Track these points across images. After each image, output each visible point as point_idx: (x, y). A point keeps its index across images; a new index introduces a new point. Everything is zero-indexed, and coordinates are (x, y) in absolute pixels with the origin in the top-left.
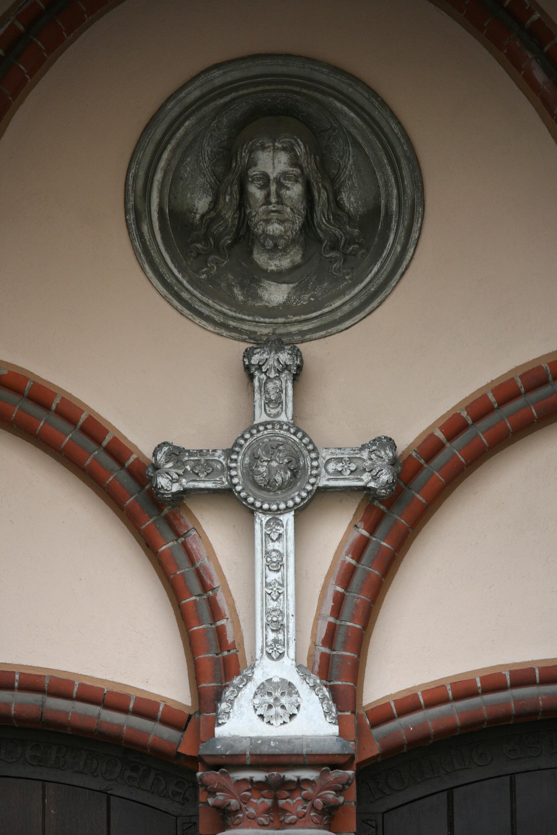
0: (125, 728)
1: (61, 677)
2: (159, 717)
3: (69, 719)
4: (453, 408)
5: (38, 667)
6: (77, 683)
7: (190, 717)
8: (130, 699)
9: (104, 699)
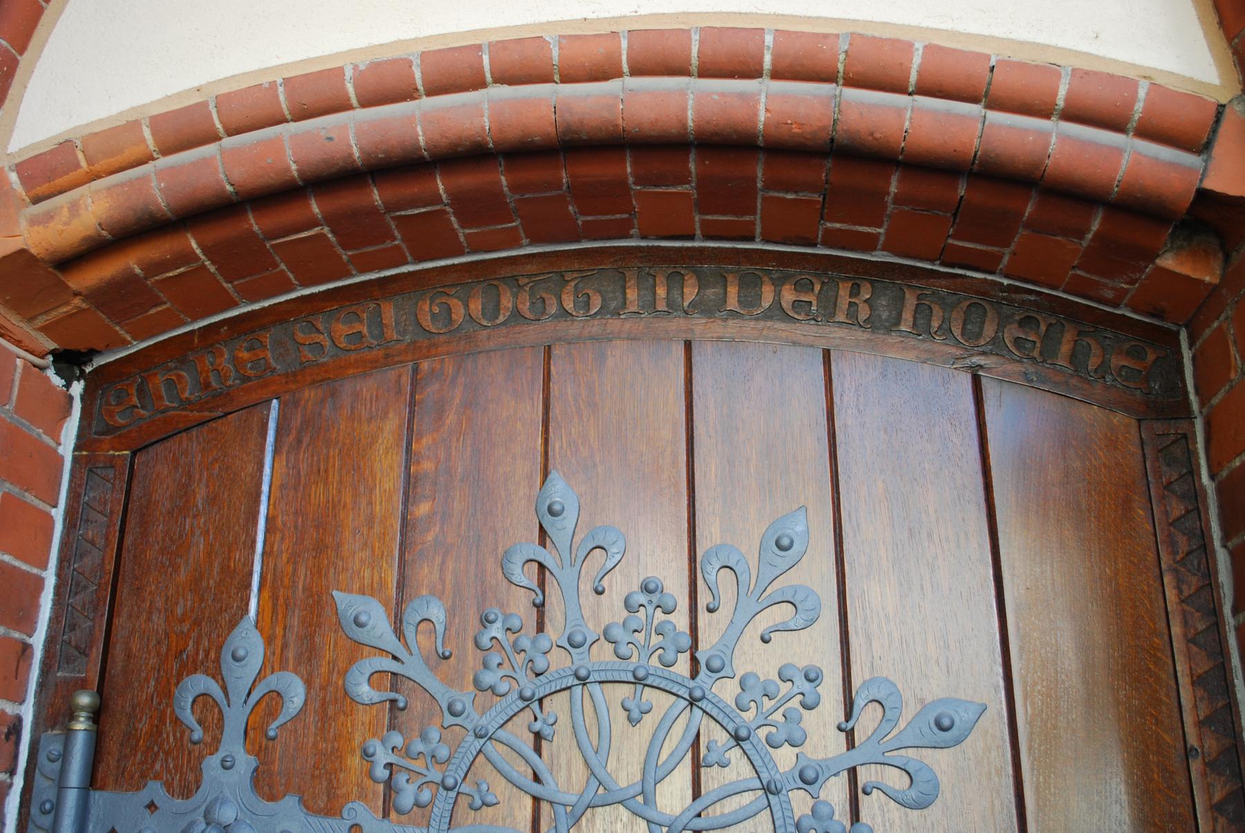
0: (1054, 140)
1: (877, 34)
2: (1136, 117)
3: (907, 124)
4: (541, 25)
5: (818, 18)
6: (919, 46)
7: (1220, 109)
8: (1059, 76)
9: (990, 84)
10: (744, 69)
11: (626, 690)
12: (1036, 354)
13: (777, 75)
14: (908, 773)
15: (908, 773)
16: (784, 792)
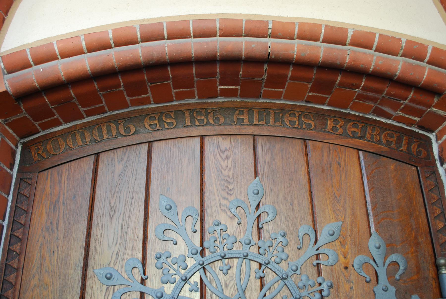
10: (184, 35)
11: (219, 263)
12: (158, 127)
13: (195, 37)
14: (133, 268)
15: (133, 268)
16: (249, 253)
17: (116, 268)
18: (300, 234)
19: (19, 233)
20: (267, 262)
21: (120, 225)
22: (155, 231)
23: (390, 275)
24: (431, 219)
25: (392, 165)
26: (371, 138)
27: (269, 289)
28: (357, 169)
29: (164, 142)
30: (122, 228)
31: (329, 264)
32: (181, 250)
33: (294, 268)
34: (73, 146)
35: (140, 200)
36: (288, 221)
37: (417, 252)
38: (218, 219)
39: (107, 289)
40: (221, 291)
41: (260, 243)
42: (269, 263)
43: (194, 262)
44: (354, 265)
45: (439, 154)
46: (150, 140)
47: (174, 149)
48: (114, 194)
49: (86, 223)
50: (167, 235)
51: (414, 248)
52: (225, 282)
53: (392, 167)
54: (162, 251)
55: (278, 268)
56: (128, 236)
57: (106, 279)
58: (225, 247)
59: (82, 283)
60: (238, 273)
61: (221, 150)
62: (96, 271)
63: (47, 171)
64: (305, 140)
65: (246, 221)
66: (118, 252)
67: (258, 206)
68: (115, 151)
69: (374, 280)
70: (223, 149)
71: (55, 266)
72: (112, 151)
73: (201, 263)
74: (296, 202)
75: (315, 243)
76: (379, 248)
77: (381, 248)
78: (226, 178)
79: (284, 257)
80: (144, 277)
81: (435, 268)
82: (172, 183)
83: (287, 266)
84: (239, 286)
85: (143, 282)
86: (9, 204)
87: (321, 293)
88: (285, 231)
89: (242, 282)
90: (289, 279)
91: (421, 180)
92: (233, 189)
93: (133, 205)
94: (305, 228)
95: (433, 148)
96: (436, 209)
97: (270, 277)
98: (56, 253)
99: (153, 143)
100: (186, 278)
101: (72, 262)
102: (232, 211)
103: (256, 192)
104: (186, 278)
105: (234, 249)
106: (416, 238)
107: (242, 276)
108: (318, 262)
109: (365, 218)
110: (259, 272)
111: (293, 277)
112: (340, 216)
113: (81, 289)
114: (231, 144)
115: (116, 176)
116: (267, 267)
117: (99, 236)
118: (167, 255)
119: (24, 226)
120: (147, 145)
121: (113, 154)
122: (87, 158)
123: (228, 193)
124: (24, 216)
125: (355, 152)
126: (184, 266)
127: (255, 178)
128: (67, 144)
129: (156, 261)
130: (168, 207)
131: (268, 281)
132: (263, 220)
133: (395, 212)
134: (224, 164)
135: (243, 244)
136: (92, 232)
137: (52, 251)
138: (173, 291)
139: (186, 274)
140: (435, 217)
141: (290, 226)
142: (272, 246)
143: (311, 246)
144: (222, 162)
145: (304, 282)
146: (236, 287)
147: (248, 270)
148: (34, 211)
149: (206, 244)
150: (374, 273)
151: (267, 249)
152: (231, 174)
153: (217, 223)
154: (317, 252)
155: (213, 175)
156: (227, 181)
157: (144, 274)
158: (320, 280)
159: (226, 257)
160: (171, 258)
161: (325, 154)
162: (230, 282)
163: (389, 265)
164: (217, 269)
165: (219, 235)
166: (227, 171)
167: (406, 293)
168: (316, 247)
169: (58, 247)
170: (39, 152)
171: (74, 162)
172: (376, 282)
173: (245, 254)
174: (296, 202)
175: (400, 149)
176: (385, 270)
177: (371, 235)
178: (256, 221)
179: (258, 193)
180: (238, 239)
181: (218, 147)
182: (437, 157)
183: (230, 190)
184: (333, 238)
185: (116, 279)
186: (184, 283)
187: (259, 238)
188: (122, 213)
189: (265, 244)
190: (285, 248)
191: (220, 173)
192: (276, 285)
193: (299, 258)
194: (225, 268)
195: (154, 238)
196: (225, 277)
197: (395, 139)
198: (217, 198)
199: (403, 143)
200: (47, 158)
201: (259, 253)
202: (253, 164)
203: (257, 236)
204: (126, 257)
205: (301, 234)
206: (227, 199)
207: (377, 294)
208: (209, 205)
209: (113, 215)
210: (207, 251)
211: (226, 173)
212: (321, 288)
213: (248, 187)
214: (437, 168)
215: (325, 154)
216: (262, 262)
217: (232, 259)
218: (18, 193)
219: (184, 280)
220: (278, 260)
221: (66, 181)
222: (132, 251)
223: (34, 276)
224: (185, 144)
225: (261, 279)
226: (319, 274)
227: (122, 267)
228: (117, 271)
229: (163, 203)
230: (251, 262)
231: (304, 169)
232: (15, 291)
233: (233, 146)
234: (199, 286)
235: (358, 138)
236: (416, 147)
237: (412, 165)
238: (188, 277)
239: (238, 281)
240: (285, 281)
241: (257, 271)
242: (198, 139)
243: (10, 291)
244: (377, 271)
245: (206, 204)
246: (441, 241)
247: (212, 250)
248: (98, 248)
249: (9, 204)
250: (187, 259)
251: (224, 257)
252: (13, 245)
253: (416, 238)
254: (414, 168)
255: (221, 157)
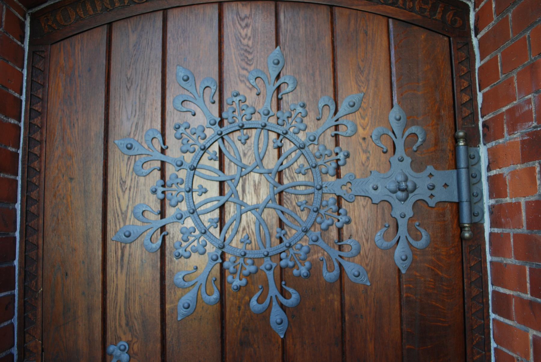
11: (237, 134)
16: (267, 123)
17: (136, 138)
18: (320, 105)
19: (38, 107)
20: (284, 132)
21: (138, 97)
22: (173, 102)
23: (407, 146)
24: (457, 92)
25: (423, 35)
26: (403, 5)
27: (286, 158)
28: (385, 38)
29: (179, 9)
30: (140, 100)
31: (348, 135)
32: (200, 120)
33: (312, 138)
34: (84, 15)
35: (157, 71)
36: (308, 92)
37: (438, 124)
38: (236, 90)
39: (129, 158)
40: (239, 160)
41: (279, 114)
42: (287, 133)
43: (213, 132)
44: (373, 137)
45: (475, 23)
46: (164, 7)
47: (191, 17)
48: (130, 66)
49: (104, 95)
50: (186, 106)
51: (435, 121)
52: (243, 151)
53: (423, 37)
54: (180, 122)
55: (295, 138)
56: (147, 107)
57: (126, 149)
58: (244, 118)
59: (104, 153)
60: (256, 143)
61: (240, 18)
62: (116, 142)
63: (59, 43)
64: (331, 7)
65: (265, 92)
66: (137, 124)
67: (278, 77)
68: (128, 20)
69: (391, 150)
70: (243, 16)
71: (77, 138)
72: (125, 20)
73: (219, 133)
74: (317, 73)
75: (335, 113)
76: (399, 119)
77: (401, 120)
78: (245, 48)
79: (302, 127)
80: (163, 147)
81: (454, 141)
82: (189, 53)
83: (305, 136)
84: (257, 155)
85: (163, 151)
86: (25, 78)
87: (337, 162)
88: (305, 102)
89: (260, 151)
90: (306, 148)
91: (453, 52)
92: (252, 59)
93: (150, 76)
94: (326, 99)
95: (471, 16)
96: (464, 82)
97: (288, 146)
98: (76, 125)
99: (168, 10)
100: (205, 147)
101: (93, 134)
102: (251, 81)
103: (276, 62)
104: (205, 147)
105: (253, 119)
106: (439, 111)
107: (260, 146)
108: (336, 132)
109: (388, 89)
110: (277, 142)
111: (311, 147)
112: (362, 88)
113: (104, 159)
114: (251, 11)
115: (131, 47)
116: (284, 137)
117: (117, 108)
118: (185, 125)
119: (42, 99)
120: (161, 13)
121: (126, 24)
122: (100, 29)
123: (247, 64)
124: (41, 90)
125: (384, 20)
126: (203, 136)
127: (276, 46)
128: (77, 13)
129: (175, 132)
130: (185, 78)
131: (286, 151)
132: (283, 91)
133: (420, 84)
134: (243, 32)
135: (262, 114)
136: (110, 105)
137: (72, 124)
138: (192, 159)
139: (205, 144)
140: (462, 90)
141: (311, 97)
142: (291, 117)
143: (330, 118)
144: (241, 31)
145: (321, 151)
146: (254, 155)
147: (266, 140)
148: (50, 85)
149: (224, 115)
150: (392, 144)
151: (286, 120)
152: (250, 43)
153: (235, 94)
154: (336, 123)
155: (231, 44)
156: (246, 51)
157: (164, 144)
158: (337, 150)
159: (245, 127)
160: (190, 129)
161: (352, 22)
162: (248, 152)
163: (408, 137)
164: (236, 139)
165: (238, 105)
166: (246, 40)
167: (422, 164)
168: (335, 118)
169: (77, 120)
170: (49, 24)
171: (86, 33)
172: (393, 153)
173: (263, 124)
174: (317, 73)
175: (434, 18)
176: (403, 142)
177: (392, 106)
178: (276, 92)
179: (278, 63)
180: (257, 109)
181: (238, 14)
182: (472, 27)
183: (250, 60)
184: (353, 109)
185: (136, 149)
186: (202, 152)
187: (279, 109)
188: (139, 85)
189: (283, 115)
190: (305, 119)
191: (240, 43)
192: (293, 155)
193: (318, 128)
194: (243, 138)
195: (172, 109)
196: (243, 146)
197: (430, 6)
198: (236, 68)
199: (438, 11)
200: (58, 29)
201: (278, 124)
202: (274, 32)
203: (276, 107)
204: (145, 128)
205: (321, 105)
206: (246, 70)
207: (392, 164)
208: (228, 75)
209: (130, 87)
210: (225, 122)
211: (245, 42)
212: (338, 157)
213: (268, 56)
214: (471, 39)
215: (352, 22)
216: (280, 132)
217: (250, 130)
218: (32, 67)
219: (202, 150)
220: (296, 131)
221: (80, 53)
222: (151, 122)
223: (57, 148)
224: (202, 11)
225: (279, 148)
226: (337, 144)
227: (142, 138)
228: (138, 141)
229: (180, 74)
230: (270, 132)
231: (327, 40)
232: (40, 162)
233: (253, 12)
234: (218, 155)
235: (390, 5)
236: (451, 16)
237: (445, 35)
238: (207, 146)
239: (256, 151)
240: (302, 150)
241: (275, 141)
242: (216, 6)
243: (36, 163)
244: (395, 143)
245: (225, 75)
246: (464, 115)
247: (230, 121)
248: (118, 120)
249: (25, 78)
250: (206, 129)
251: (242, 127)
252: (33, 119)
253: (439, 111)
254: (446, 39)
255: (240, 25)
